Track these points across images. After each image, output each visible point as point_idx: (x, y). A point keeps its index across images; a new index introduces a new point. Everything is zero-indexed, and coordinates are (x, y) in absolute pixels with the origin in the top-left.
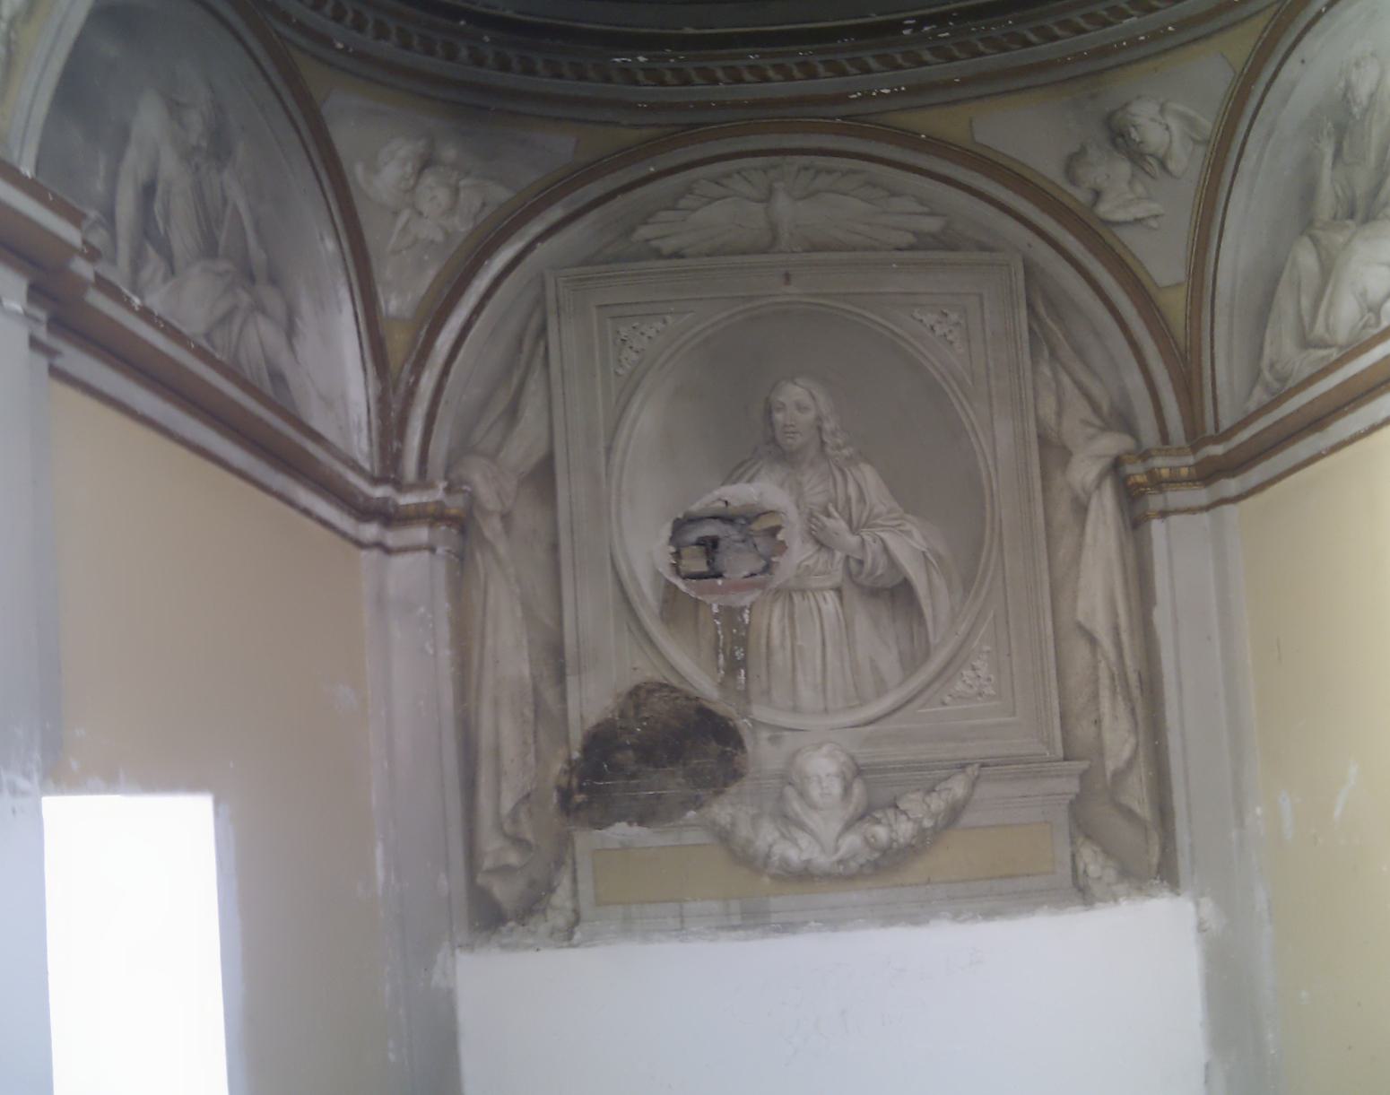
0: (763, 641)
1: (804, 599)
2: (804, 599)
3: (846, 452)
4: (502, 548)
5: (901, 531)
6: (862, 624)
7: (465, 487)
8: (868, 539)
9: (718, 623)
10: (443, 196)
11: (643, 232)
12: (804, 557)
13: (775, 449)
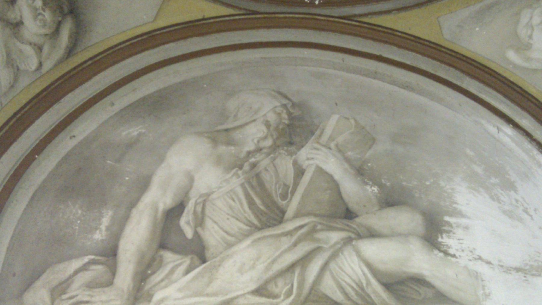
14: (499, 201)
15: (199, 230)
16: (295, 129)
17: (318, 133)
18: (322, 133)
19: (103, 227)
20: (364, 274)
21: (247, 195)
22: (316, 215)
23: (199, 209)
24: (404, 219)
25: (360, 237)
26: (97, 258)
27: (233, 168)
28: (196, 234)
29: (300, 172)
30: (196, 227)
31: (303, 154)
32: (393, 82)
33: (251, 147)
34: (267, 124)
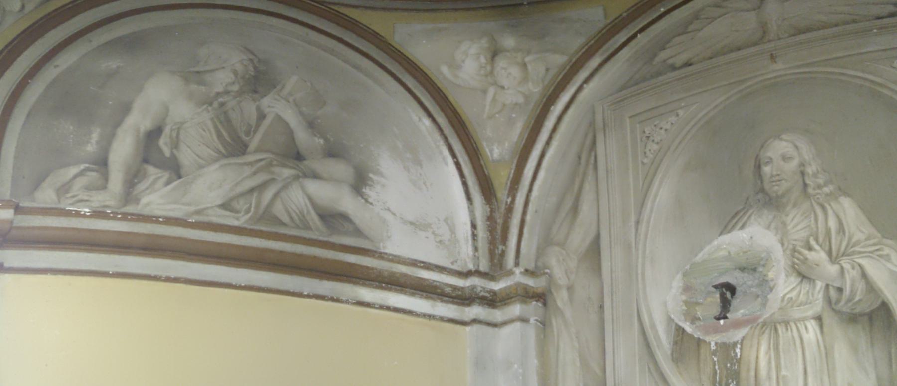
0: (753, 373)
1: (787, 329)
2: (787, 329)
3: (826, 189)
4: (568, 313)
5: (880, 256)
6: (841, 353)
7: (547, 271)
8: (847, 266)
9: (715, 359)
10: (515, 71)
11: (663, 55)
12: (786, 291)
13: (768, 199)
14: (408, 170)
15: (175, 151)
16: (259, 80)
17: (278, 87)
18: (283, 87)
19: (93, 141)
20: (306, 205)
21: (216, 127)
22: (273, 153)
23: (174, 134)
24: (341, 169)
25: (306, 176)
26: (91, 166)
27: (204, 104)
28: (172, 153)
29: (262, 116)
30: (172, 149)
31: (265, 102)
32: (346, 61)
33: (220, 89)
34: (235, 73)
